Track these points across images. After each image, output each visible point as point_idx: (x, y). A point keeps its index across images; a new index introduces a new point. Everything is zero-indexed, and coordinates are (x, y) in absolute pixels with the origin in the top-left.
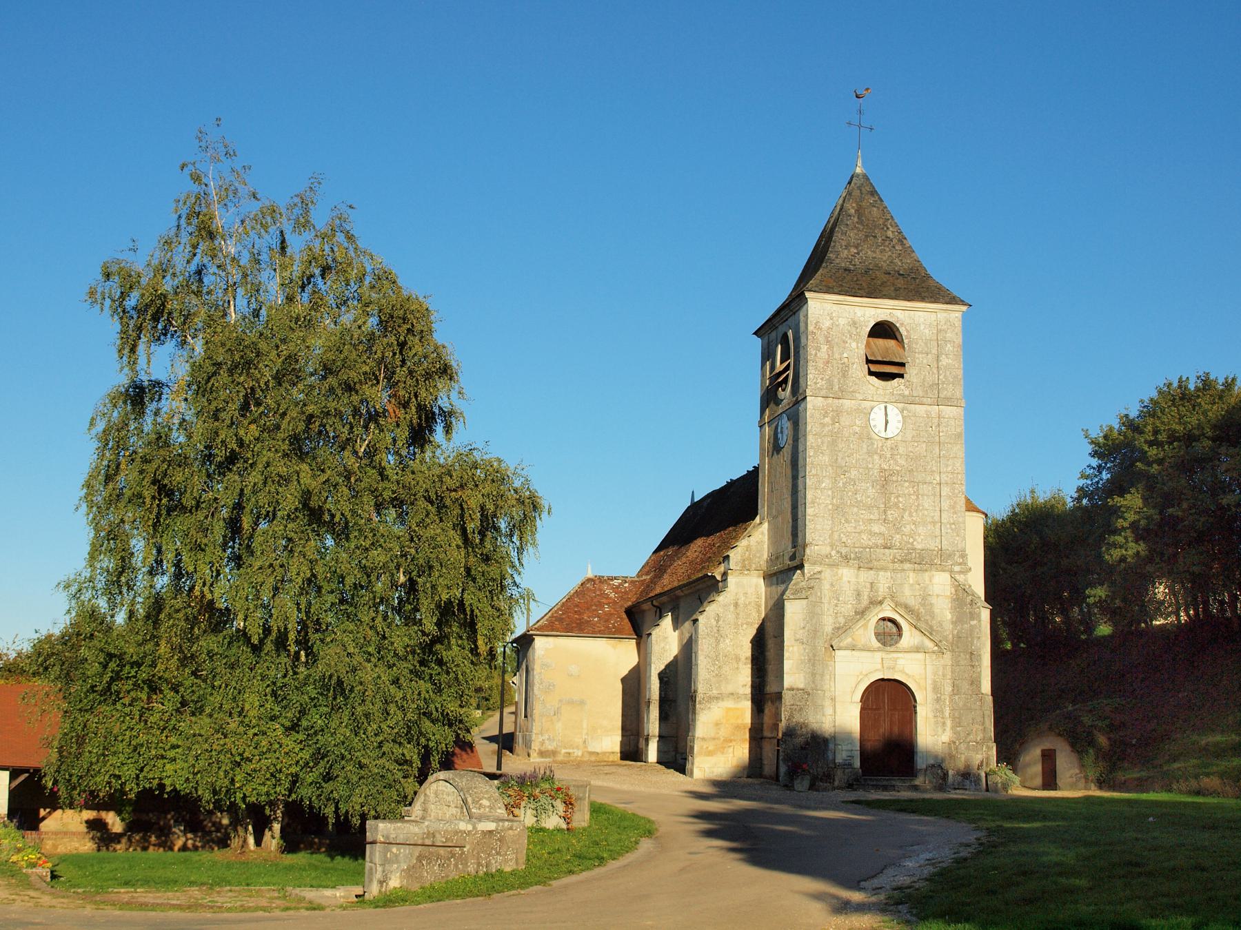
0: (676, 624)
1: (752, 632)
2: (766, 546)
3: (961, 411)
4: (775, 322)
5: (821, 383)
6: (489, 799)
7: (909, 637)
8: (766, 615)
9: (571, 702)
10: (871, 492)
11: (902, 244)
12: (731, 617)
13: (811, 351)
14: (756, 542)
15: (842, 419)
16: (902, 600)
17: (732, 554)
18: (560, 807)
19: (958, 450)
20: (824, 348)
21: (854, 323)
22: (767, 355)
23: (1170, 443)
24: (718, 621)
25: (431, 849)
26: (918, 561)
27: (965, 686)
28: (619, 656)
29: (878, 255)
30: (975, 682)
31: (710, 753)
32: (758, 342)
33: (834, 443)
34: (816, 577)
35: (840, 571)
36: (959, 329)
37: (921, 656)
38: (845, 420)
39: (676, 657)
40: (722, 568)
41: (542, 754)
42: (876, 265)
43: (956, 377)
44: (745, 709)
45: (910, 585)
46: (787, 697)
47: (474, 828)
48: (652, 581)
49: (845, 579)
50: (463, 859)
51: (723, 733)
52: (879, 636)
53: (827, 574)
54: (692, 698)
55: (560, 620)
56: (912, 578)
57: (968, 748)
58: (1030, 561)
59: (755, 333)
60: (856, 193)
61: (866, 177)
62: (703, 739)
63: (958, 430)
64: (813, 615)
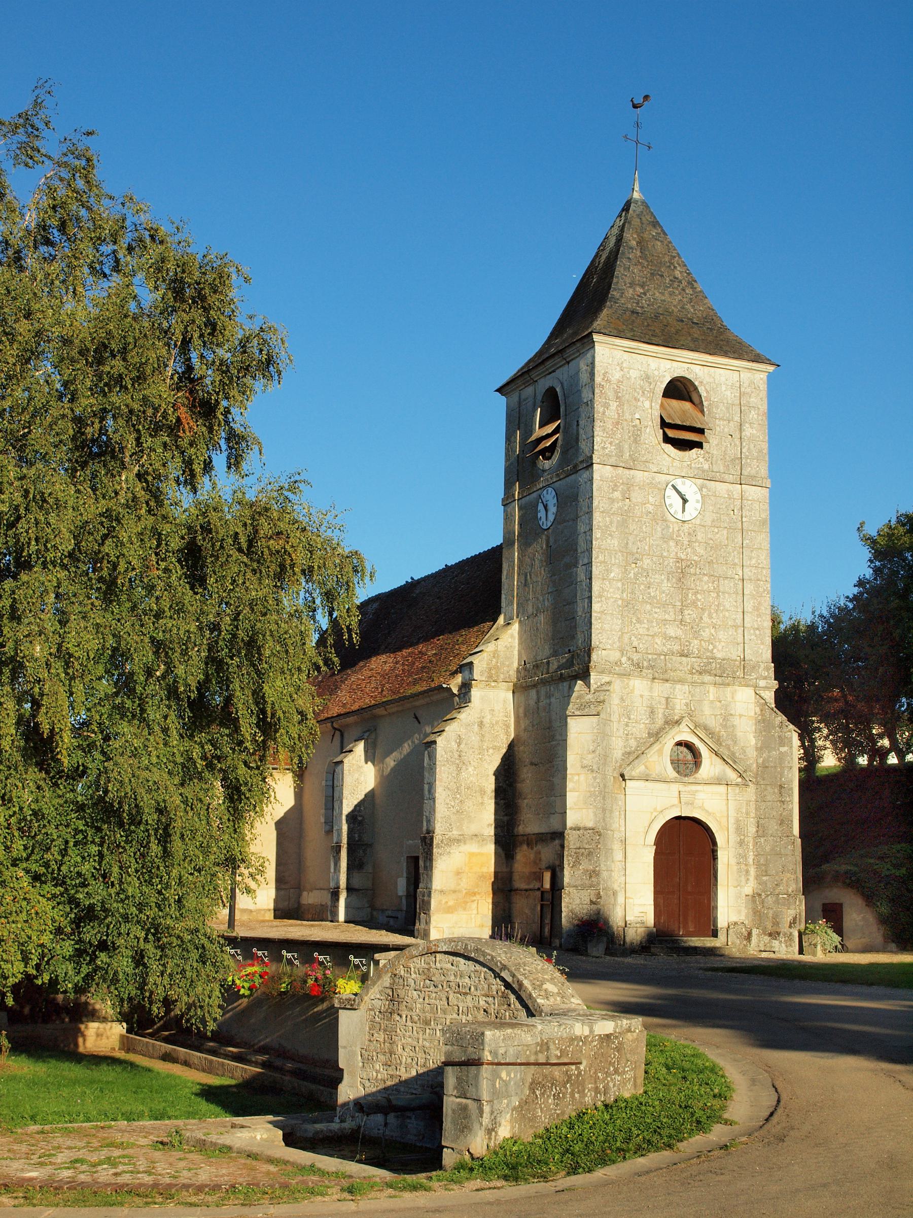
0: (370, 757)
1: (495, 761)
2: (516, 653)
3: (766, 492)
7: (710, 766)
10: (666, 586)
11: (693, 288)
12: (474, 739)
13: (599, 408)
14: (502, 650)
16: (701, 720)
17: (476, 660)
19: (763, 540)
20: (614, 405)
21: (648, 377)
22: (517, 421)
24: (459, 744)
25: (547, 1070)
26: (718, 672)
27: (773, 827)
29: (666, 297)
30: (784, 822)
31: (449, 910)
33: (623, 524)
34: (605, 688)
35: (631, 683)
36: (764, 394)
37: (723, 788)
38: (637, 496)
40: (459, 679)
43: (760, 451)
46: (571, 839)
47: (591, 1031)
50: (579, 1085)
51: (465, 883)
52: (676, 763)
53: (617, 686)
57: (777, 902)
59: (499, 390)
61: (643, 202)
63: (763, 516)
64: (602, 735)
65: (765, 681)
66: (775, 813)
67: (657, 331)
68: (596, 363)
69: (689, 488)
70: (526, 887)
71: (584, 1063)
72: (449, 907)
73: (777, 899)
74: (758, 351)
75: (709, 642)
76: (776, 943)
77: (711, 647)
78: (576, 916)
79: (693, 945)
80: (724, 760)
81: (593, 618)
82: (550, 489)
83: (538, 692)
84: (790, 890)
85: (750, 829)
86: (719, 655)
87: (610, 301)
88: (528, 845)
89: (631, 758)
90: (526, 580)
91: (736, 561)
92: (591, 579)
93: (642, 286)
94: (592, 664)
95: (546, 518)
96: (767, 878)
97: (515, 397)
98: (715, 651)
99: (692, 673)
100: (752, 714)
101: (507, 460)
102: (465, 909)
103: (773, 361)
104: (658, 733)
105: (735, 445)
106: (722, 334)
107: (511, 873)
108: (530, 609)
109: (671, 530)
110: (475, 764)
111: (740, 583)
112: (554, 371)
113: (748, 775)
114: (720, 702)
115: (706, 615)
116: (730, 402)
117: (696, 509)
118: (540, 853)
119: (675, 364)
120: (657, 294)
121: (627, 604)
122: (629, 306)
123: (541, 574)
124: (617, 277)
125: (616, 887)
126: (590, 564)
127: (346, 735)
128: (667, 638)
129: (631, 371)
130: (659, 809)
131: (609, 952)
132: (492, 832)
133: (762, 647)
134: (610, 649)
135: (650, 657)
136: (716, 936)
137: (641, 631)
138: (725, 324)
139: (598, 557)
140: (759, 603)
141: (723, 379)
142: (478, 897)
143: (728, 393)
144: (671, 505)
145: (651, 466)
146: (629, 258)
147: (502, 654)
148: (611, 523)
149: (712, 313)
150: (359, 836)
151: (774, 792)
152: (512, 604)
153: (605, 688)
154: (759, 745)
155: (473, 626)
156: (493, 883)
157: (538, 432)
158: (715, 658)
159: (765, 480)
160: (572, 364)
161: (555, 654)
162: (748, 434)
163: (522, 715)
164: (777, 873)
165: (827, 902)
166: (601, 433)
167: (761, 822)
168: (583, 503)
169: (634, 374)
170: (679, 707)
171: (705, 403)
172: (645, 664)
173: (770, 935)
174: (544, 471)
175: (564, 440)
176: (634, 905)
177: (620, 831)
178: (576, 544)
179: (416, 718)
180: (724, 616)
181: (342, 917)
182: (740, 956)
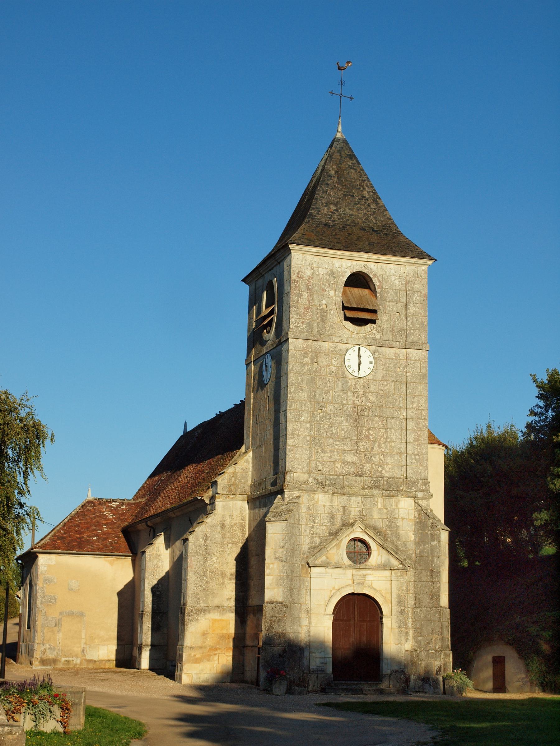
1: (236, 551)
3: (425, 353)
7: (377, 556)
8: (250, 536)
9: (71, 614)
10: (345, 425)
11: (377, 203)
12: (218, 536)
13: (294, 297)
14: (242, 468)
15: (320, 360)
16: (371, 522)
17: (219, 479)
19: (422, 389)
20: (305, 295)
24: (206, 540)
27: (426, 600)
29: (355, 212)
30: (435, 596)
31: (197, 661)
32: (245, 289)
33: (312, 381)
34: (295, 501)
35: (316, 496)
36: (425, 281)
37: (387, 573)
38: (323, 360)
40: (210, 493)
41: (43, 662)
42: (353, 222)
43: (422, 324)
45: (378, 508)
46: (267, 610)
49: (320, 503)
51: (210, 642)
53: (305, 499)
55: (62, 538)
56: (380, 502)
57: (428, 655)
60: (337, 156)
62: (191, 648)
63: (423, 371)
64: (291, 535)
65: (422, 493)
72: (197, 659)
73: (428, 654)
77: (380, 469)
80: (389, 552)
81: (287, 450)
83: (260, 502)
84: (437, 647)
85: (409, 602)
88: (253, 614)
91: (401, 405)
92: (286, 422)
93: (336, 205)
94: (286, 483)
96: (422, 638)
98: (383, 472)
99: (364, 489)
100: (412, 517)
102: (209, 660)
105: (402, 320)
106: (395, 237)
107: (245, 634)
108: (258, 442)
109: (349, 384)
110: (218, 555)
111: (404, 421)
112: (272, 269)
114: (386, 509)
115: (376, 445)
116: (398, 288)
117: (370, 368)
119: (354, 263)
120: (347, 210)
122: (323, 221)
124: (316, 199)
126: (286, 411)
128: (345, 463)
129: (320, 269)
130: (337, 588)
133: (421, 468)
134: (300, 473)
135: (331, 477)
137: (325, 459)
140: (419, 436)
141: (393, 272)
142: (219, 651)
143: (397, 282)
144: (349, 366)
145: (334, 338)
146: (328, 184)
147: (239, 475)
148: (302, 381)
149: (390, 222)
151: (427, 575)
153: (295, 501)
154: (417, 540)
158: (383, 477)
159: (425, 345)
160: (281, 264)
162: (412, 311)
164: (428, 634)
166: (295, 316)
167: (418, 596)
169: (321, 271)
170: (354, 512)
171: (378, 290)
172: (328, 482)
177: (306, 604)
179: (190, 520)
180: (391, 446)
181: (145, 662)
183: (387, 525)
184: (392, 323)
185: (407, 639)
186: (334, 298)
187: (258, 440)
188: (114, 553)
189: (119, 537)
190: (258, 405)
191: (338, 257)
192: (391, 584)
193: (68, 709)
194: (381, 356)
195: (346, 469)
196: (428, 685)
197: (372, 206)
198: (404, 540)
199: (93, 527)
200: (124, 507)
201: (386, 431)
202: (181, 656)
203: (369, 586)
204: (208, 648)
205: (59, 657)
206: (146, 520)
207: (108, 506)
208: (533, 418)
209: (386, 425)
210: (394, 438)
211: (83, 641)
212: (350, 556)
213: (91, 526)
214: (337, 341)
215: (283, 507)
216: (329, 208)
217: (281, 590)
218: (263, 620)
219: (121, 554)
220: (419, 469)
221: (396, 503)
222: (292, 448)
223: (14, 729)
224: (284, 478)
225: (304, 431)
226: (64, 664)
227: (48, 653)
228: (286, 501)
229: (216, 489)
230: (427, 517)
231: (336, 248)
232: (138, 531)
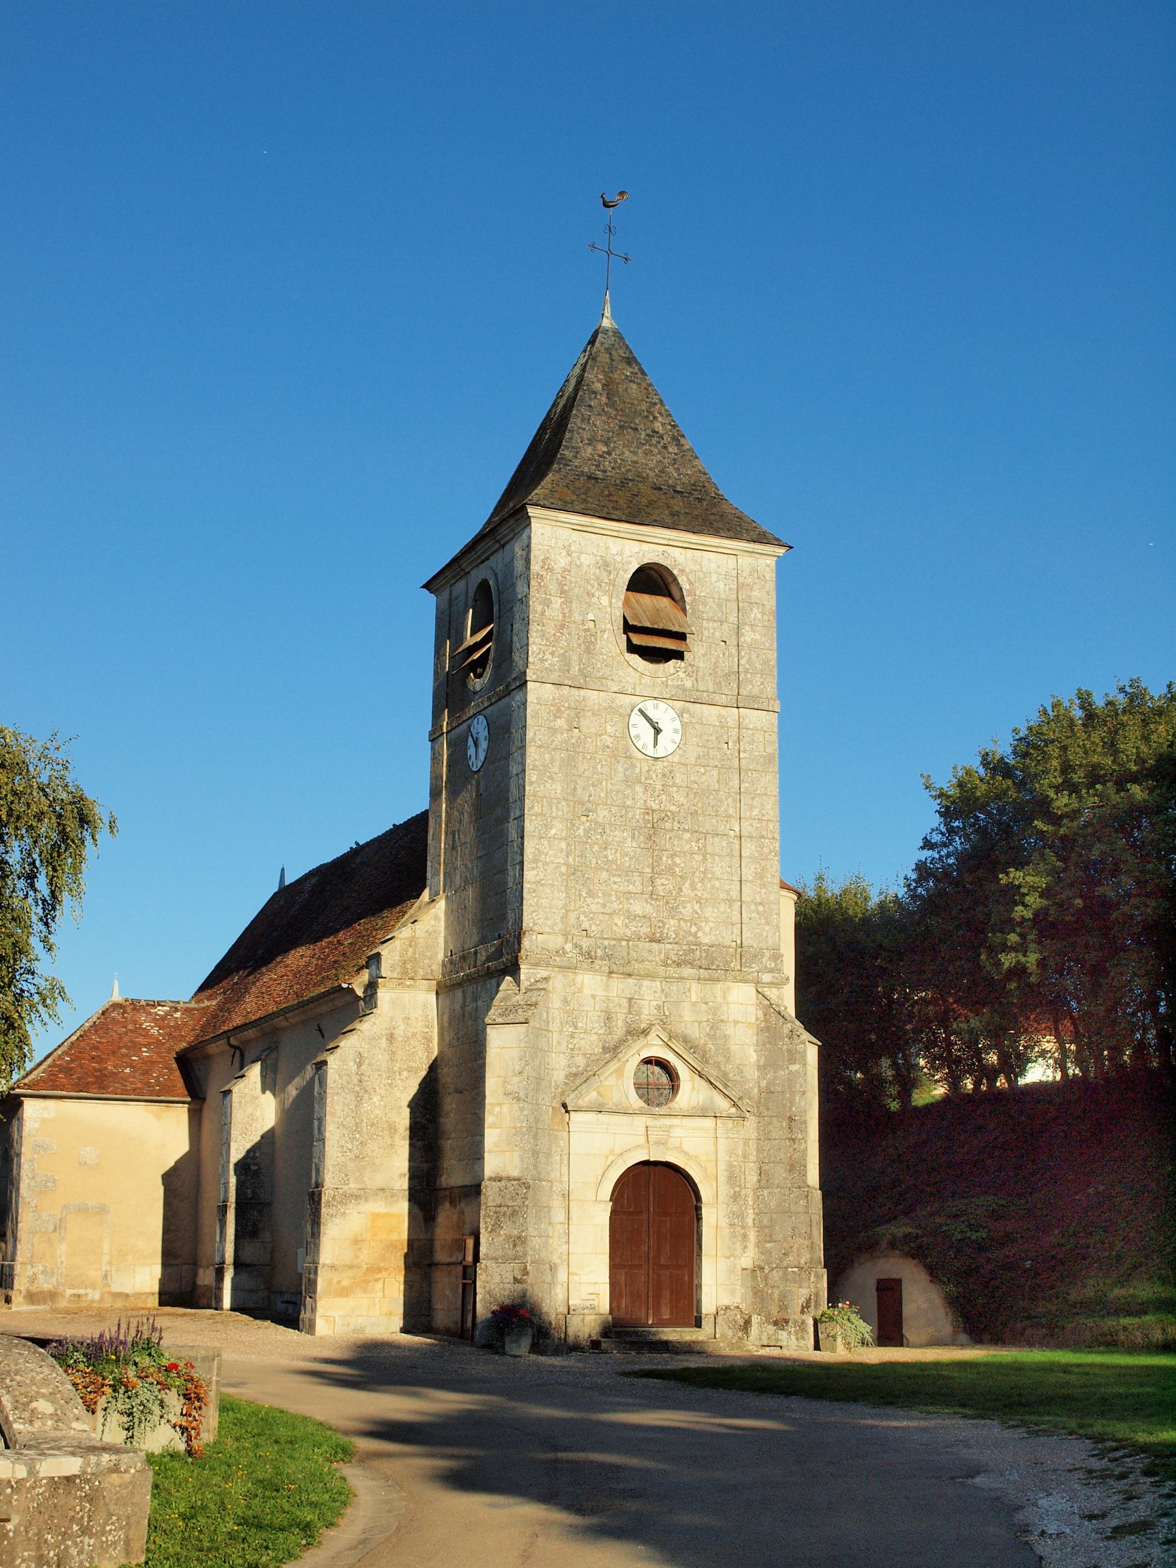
0: (269, 1083)
1: (410, 1087)
2: (441, 940)
4: (480, 548)
5: (551, 660)
6: (51, 1397)
7: (691, 1092)
8: (441, 1053)
9: (83, 1210)
10: (630, 845)
11: (679, 445)
12: (382, 1058)
14: (425, 933)
16: (680, 1028)
17: (385, 951)
18: (174, 1400)
19: (769, 782)
20: (557, 602)
22: (447, 627)
23: (1091, 785)
24: (359, 1065)
26: (704, 963)
27: (780, 1174)
28: (164, 1132)
29: (640, 458)
30: (796, 1167)
31: (344, 1292)
32: (429, 603)
34: (540, 986)
35: (579, 978)
36: (771, 586)
37: (709, 1123)
38: (589, 724)
39: (273, 1129)
40: (365, 976)
41: (32, 1297)
42: (639, 475)
43: (765, 663)
44: (397, 1214)
45: (693, 1004)
46: (490, 1192)
47: (32, 1471)
48: (221, 1008)
49: (587, 991)
51: (366, 1256)
52: (642, 1088)
53: (558, 982)
54: (315, 1198)
55: (68, 1071)
56: (695, 991)
57: (785, 1277)
58: (855, 976)
59: (426, 586)
60: (604, 358)
61: (617, 334)
63: (770, 750)
64: (535, 1051)
66: (782, 1156)
67: (621, 502)
68: (533, 546)
69: (663, 714)
70: (449, 1260)
71: (15, 1519)
72: (344, 1288)
73: (786, 1274)
74: (764, 528)
75: (693, 922)
76: (783, 1335)
77: (694, 929)
78: (496, 1300)
79: (665, 1338)
80: (711, 1083)
82: (481, 717)
83: (463, 992)
84: (802, 1262)
85: (749, 1178)
86: (706, 940)
87: (559, 463)
88: (451, 1202)
89: (578, 1082)
90: (454, 841)
91: (731, 811)
92: (522, 838)
93: (606, 444)
95: (476, 757)
96: (773, 1244)
97: (446, 593)
98: (700, 934)
99: (666, 965)
100: (753, 1020)
101: (436, 680)
102: (365, 1291)
103: (784, 541)
104: (616, 1048)
105: (730, 655)
107: (431, 1241)
108: (458, 881)
109: (637, 771)
110: (383, 1092)
111: (737, 841)
112: (487, 559)
113: (745, 1104)
114: (706, 1003)
118: (463, 1213)
119: (645, 546)
120: (627, 453)
121: (574, 871)
122: (586, 470)
123: (468, 835)
124: (572, 431)
125: (555, 1258)
126: (521, 817)
127: (247, 1054)
128: (631, 916)
129: (583, 557)
130: (617, 1151)
131: (535, 1348)
132: (406, 1186)
133: (767, 928)
134: (549, 933)
135: (606, 943)
136: (700, 1327)
137: (594, 908)
138: (720, 492)
139: (532, 808)
140: (764, 868)
141: (713, 566)
142: (384, 1274)
144: (637, 736)
145: (609, 683)
146: (590, 406)
148: (552, 761)
149: (703, 478)
150: (253, 1192)
151: (782, 1127)
152: (439, 875)
153: (540, 986)
154: (762, 1063)
155: (394, 906)
156: (406, 1256)
157: (470, 640)
158: (700, 944)
159: (772, 702)
160: (507, 547)
161: (483, 941)
162: (748, 639)
163: (446, 1024)
164: (785, 1238)
165: (883, 1277)
166: (538, 640)
168: (516, 735)
170: (647, 1011)
172: (599, 953)
173: (776, 1323)
174: (475, 693)
175: (496, 648)
176: (579, 1281)
177: (561, 1182)
178: (508, 791)
179: (320, 1030)
180: (713, 887)
181: (227, 1302)
182: (732, 1353)
183: (708, 1035)
184: (713, 660)
185: (746, 1247)
186: (609, 609)
187: (458, 877)
188: (162, 1098)
189: (170, 1069)
190: (456, 813)
191: (615, 534)
192: (716, 1144)
193: (199, 1399)
194: (694, 720)
195: (633, 929)
196: (784, 1333)
197: (670, 450)
198: (738, 1062)
199: (124, 1051)
200: (178, 1015)
201: (705, 859)
202: (312, 1284)
203: (676, 1148)
204: (365, 1267)
205: (61, 1289)
206: (227, 1034)
207: (150, 1014)
208: (927, 854)
209: (705, 847)
210: (718, 871)
211: (106, 1258)
212: (640, 1092)
213: (120, 1048)
214: (615, 689)
215: (518, 997)
216: (595, 449)
217: (516, 1154)
218: (482, 1213)
219: (176, 1099)
220: (763, 929)
221: (724, 992)
222: (534, 886)
223: (125, 1458)
224: (519, 943)
225: (555, 856)
226: (70, 1301)
227: (41, 1281)
228: (522, 987)
229: (378, 968)
230: (782, 1020)
231: (613, 516)
232: (208, 1057)
